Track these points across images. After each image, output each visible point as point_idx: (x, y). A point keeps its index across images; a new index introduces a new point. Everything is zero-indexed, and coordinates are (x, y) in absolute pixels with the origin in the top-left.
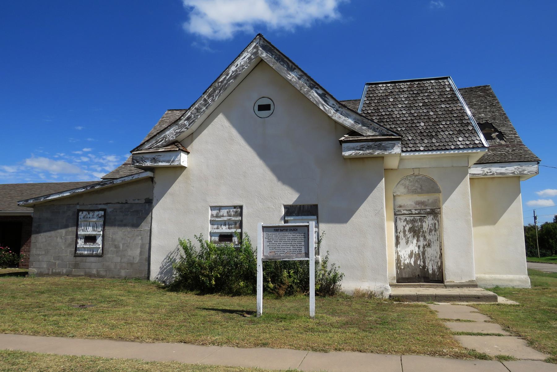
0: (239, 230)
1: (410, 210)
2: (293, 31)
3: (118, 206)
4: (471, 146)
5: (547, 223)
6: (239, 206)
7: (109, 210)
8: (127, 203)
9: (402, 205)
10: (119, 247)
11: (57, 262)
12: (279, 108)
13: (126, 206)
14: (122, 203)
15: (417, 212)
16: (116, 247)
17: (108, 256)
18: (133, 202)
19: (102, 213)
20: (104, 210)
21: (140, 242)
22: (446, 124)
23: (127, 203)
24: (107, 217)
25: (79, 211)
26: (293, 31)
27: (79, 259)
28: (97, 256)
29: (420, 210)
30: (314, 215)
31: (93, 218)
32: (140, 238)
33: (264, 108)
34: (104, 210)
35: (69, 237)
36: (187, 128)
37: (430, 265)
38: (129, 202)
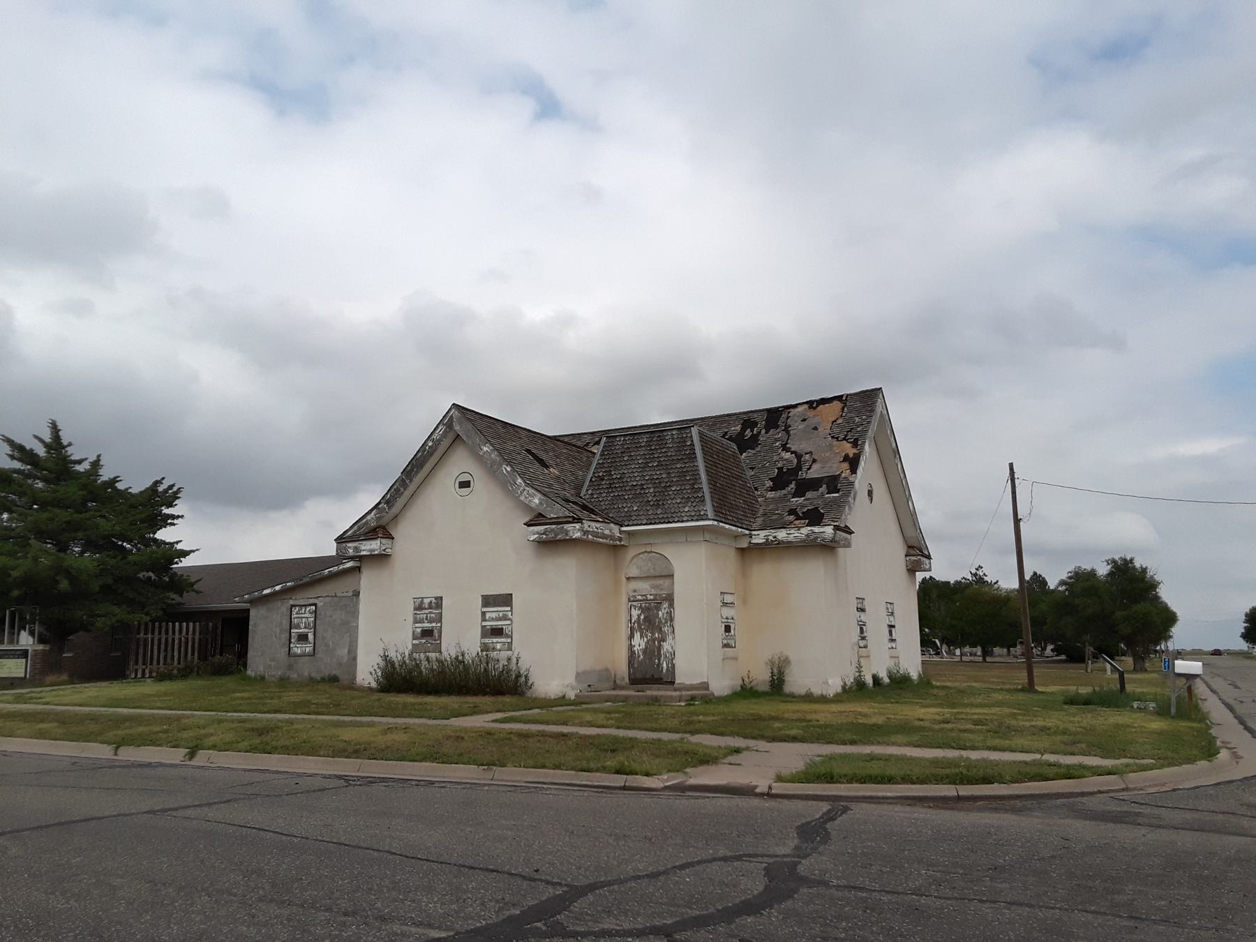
0: (439, 625)
1: (645, 595)
2: (1103, 570)
3: (328, 599)
4: (696, 518)
5: (1153, 585)
6: (1059, 585)
7: (320, 605)
8: (336, 596)
9: (637, 589)
10: (329, 646)
11: (273, 663)
12: (478, 485)
13: (336, 599)
14: (331, 596)
15: (652, 597)
16: (327, 646)
17: (319, 655)
18: (341, 595)
19: (313, 608)
20: (315, 605)
21: (348, 639)
22: (692, 502)
23: (336, 596)
24: (318, 612)
25: (292, 606)
26: (1103, 570)
27: (292, 659)
28: (309, 655)
29: (656, 595)
30: (507, 606)
31: (305, 613)
32: (348, 634)
33: (465, 485)
34: (315, 605)
35: (283, 636)
36: (387, 513)
37: (665, 663)
38: (338, 595)
